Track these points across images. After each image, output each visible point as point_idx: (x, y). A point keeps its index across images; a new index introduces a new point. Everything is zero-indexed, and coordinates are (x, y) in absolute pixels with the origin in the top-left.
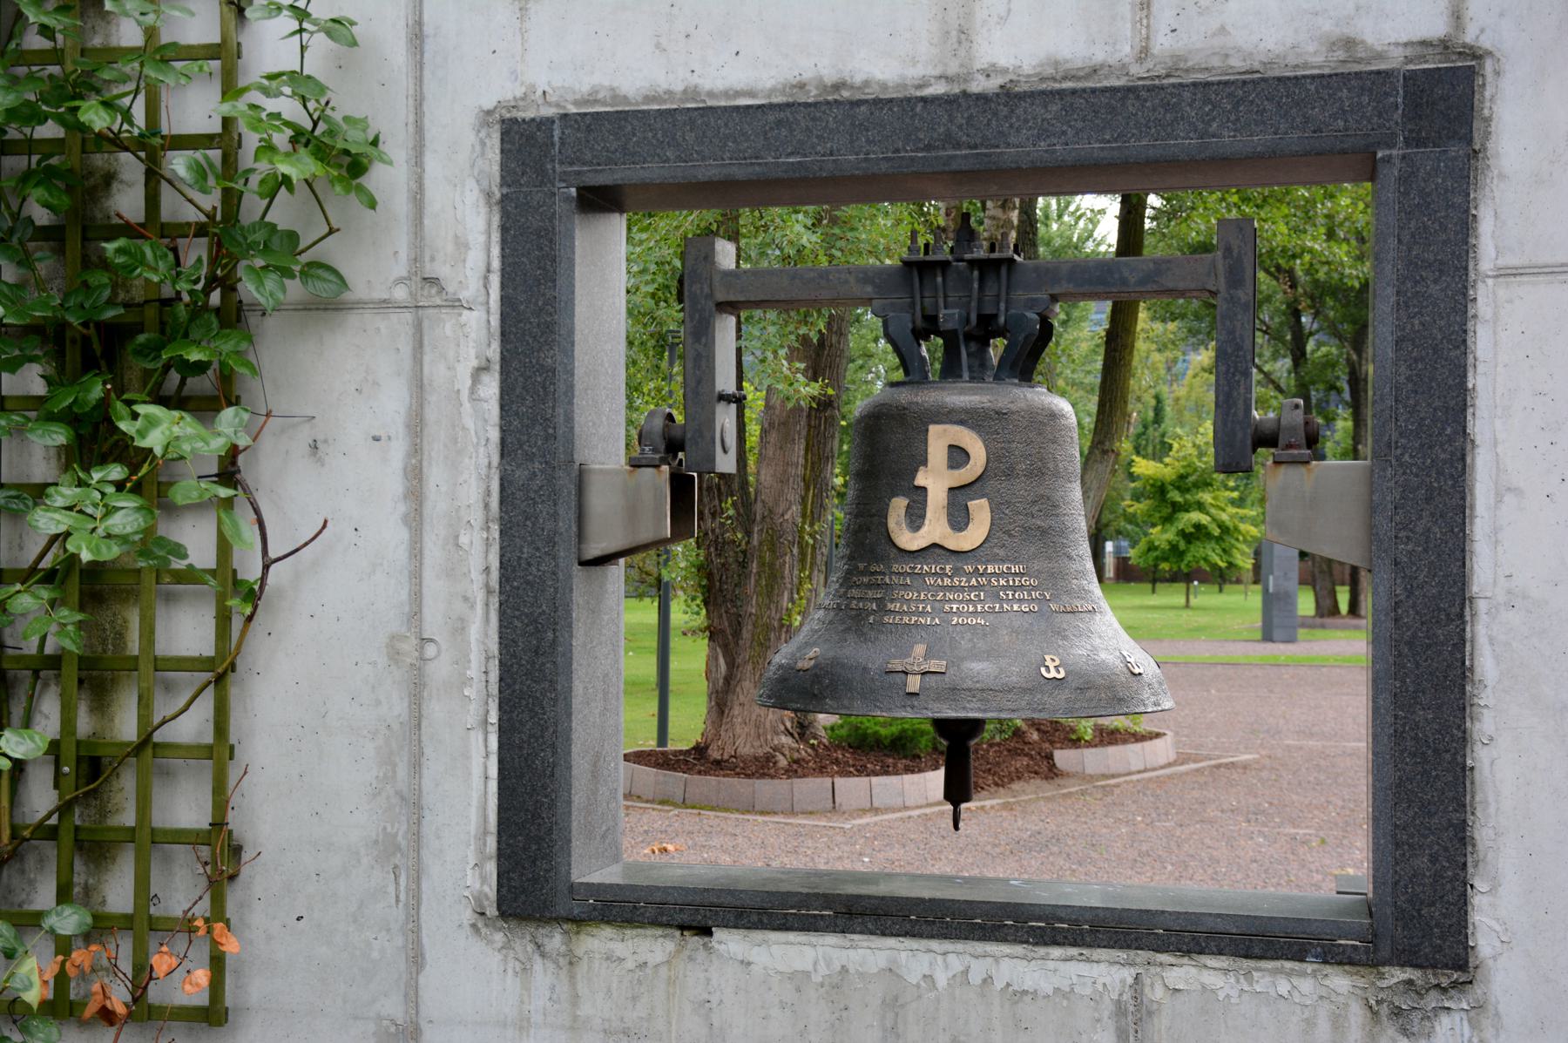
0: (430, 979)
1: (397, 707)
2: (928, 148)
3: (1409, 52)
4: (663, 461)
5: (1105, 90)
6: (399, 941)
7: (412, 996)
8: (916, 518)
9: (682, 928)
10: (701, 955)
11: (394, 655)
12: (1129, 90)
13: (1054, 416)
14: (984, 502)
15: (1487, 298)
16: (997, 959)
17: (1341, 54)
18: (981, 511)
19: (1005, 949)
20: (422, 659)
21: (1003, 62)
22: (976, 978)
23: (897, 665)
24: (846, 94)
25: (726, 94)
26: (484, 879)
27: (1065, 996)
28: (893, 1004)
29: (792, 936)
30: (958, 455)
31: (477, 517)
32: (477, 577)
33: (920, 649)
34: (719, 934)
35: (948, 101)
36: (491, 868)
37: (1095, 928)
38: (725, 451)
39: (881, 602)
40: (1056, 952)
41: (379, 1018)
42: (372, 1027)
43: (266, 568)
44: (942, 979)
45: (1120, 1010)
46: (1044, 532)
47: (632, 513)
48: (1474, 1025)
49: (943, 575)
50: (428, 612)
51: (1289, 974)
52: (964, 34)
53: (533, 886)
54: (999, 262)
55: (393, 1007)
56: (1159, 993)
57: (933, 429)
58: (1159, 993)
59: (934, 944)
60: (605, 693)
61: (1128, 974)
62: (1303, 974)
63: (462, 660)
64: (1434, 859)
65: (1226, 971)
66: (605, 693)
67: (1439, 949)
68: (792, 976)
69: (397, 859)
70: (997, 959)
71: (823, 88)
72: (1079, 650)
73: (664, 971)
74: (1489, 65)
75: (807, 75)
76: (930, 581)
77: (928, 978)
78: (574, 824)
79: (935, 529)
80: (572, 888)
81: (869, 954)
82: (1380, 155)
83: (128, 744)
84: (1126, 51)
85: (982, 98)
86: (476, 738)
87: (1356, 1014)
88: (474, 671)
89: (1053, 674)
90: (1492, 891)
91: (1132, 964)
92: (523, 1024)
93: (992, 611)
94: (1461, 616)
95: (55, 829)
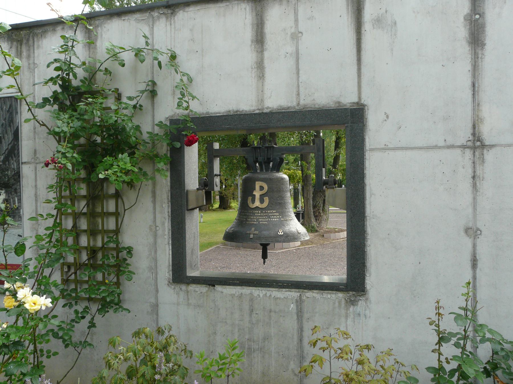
0: (160, 294)
1: (151, 240)
2: (255, 124)
3: (351, 105)
4: (203, 189)
5: (291, 112)
6: (154, 287)
7: (157, 298)
8: (253, 201)
9: (209, 285)
10: (213, 291)
11: (151, 229)
12: (295, 112)
13: (283, 179)
14: (267, 198)
15: (367, 155)
16: (272, 291)
17: (337, 105)
18: (266, 200)
19: (274, 289)
20: (156, 230)
21: (270, 106)
22: (268, 295)
23: (248, 232)
24: (239, 113)
25: (214, 113)
26: (169, 275)
27: (286, 298)
28: (251, 300)
29: (231, 287)
30: (262, 188)
31: (166, 201)
32: (167, 213)
33: (253, 229)
34: (216, 286)
35: (259, 114)
36: (171, 273)
37: (292, 285)
38: (217, 186)
39: (246, 219)
40: (284, 290)
41: (150, 302)
42: (149, 304)
43: (125, 211)
44: (261, 295)
45: (297, 301)
46: (280, 204)
47: (197, 199)
48: (366, 303)
49: (259, 213)
50: (157, 221)
51: (330, 294)
52: (262, 100)
53: (179, 275)
54: (271, 147)
55: (153, 300)
56: (305, 298)
57: (257, 182)
58: (305, 298)
59: (260, 288)
60: (194, 237)
61: (298, 294)
62: (333, 294)
63: (164, 230)
64: (359, 270)
65: (318, 293)
66: (194, 237)
67: (359, 288)
68: (231, 295)
69: (153, 271)
70: (272, 291)
71: (234, 112)
72: (287, 229)
73: (206, 294)
74: (366, 108)
75: (231, 109)
76: (256, 214)
77: (259, 295)
78: (187, 264)
79: (257, 203)
80: (187, 277)
81: (246, 290)
82: (65, 294)
83: (99, 247)
84: (295, 104)
85: (266, 113)
86: (167, 246)
87: (343, 301)
88: (166, 233)
89: (281, 234)
90: (370, 276)
91: (299, 292)
92: (178, 304)
93: (269, 221)
94: (364, 220)
95: (87, 264)
